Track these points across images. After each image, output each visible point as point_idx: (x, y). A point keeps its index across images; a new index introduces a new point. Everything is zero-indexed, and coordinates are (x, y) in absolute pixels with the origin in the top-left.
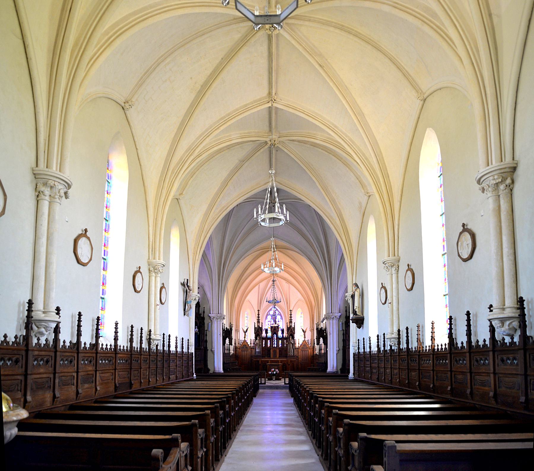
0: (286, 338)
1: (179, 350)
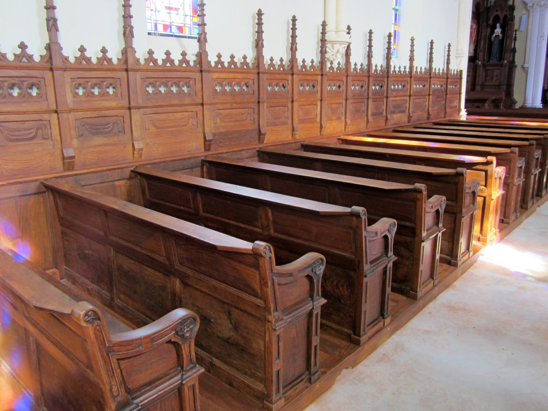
1: (378, 61)
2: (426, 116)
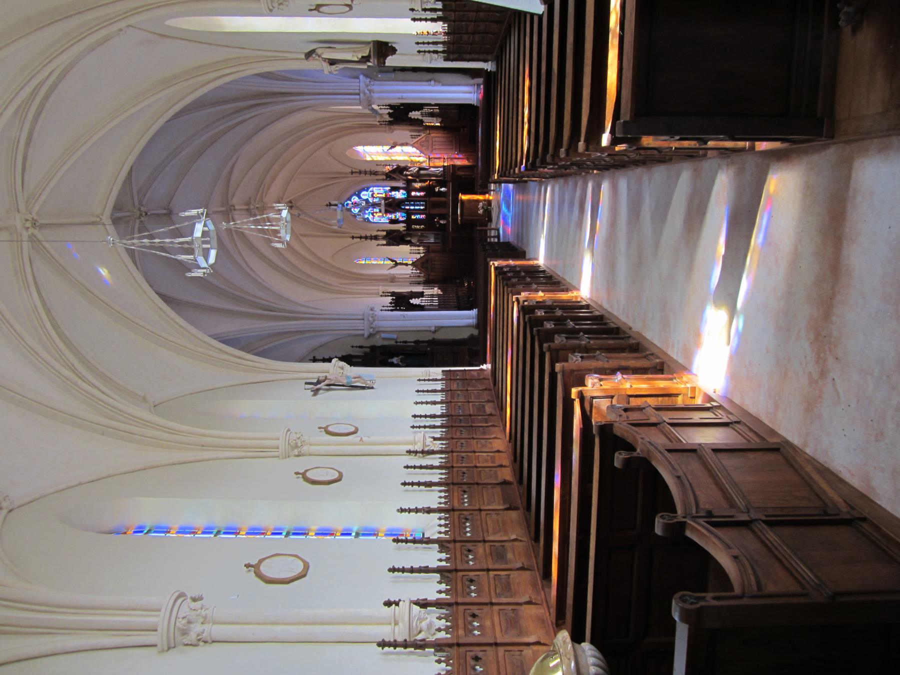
0: (409, 182)
1: (438, 397)
2: (487, 392)
